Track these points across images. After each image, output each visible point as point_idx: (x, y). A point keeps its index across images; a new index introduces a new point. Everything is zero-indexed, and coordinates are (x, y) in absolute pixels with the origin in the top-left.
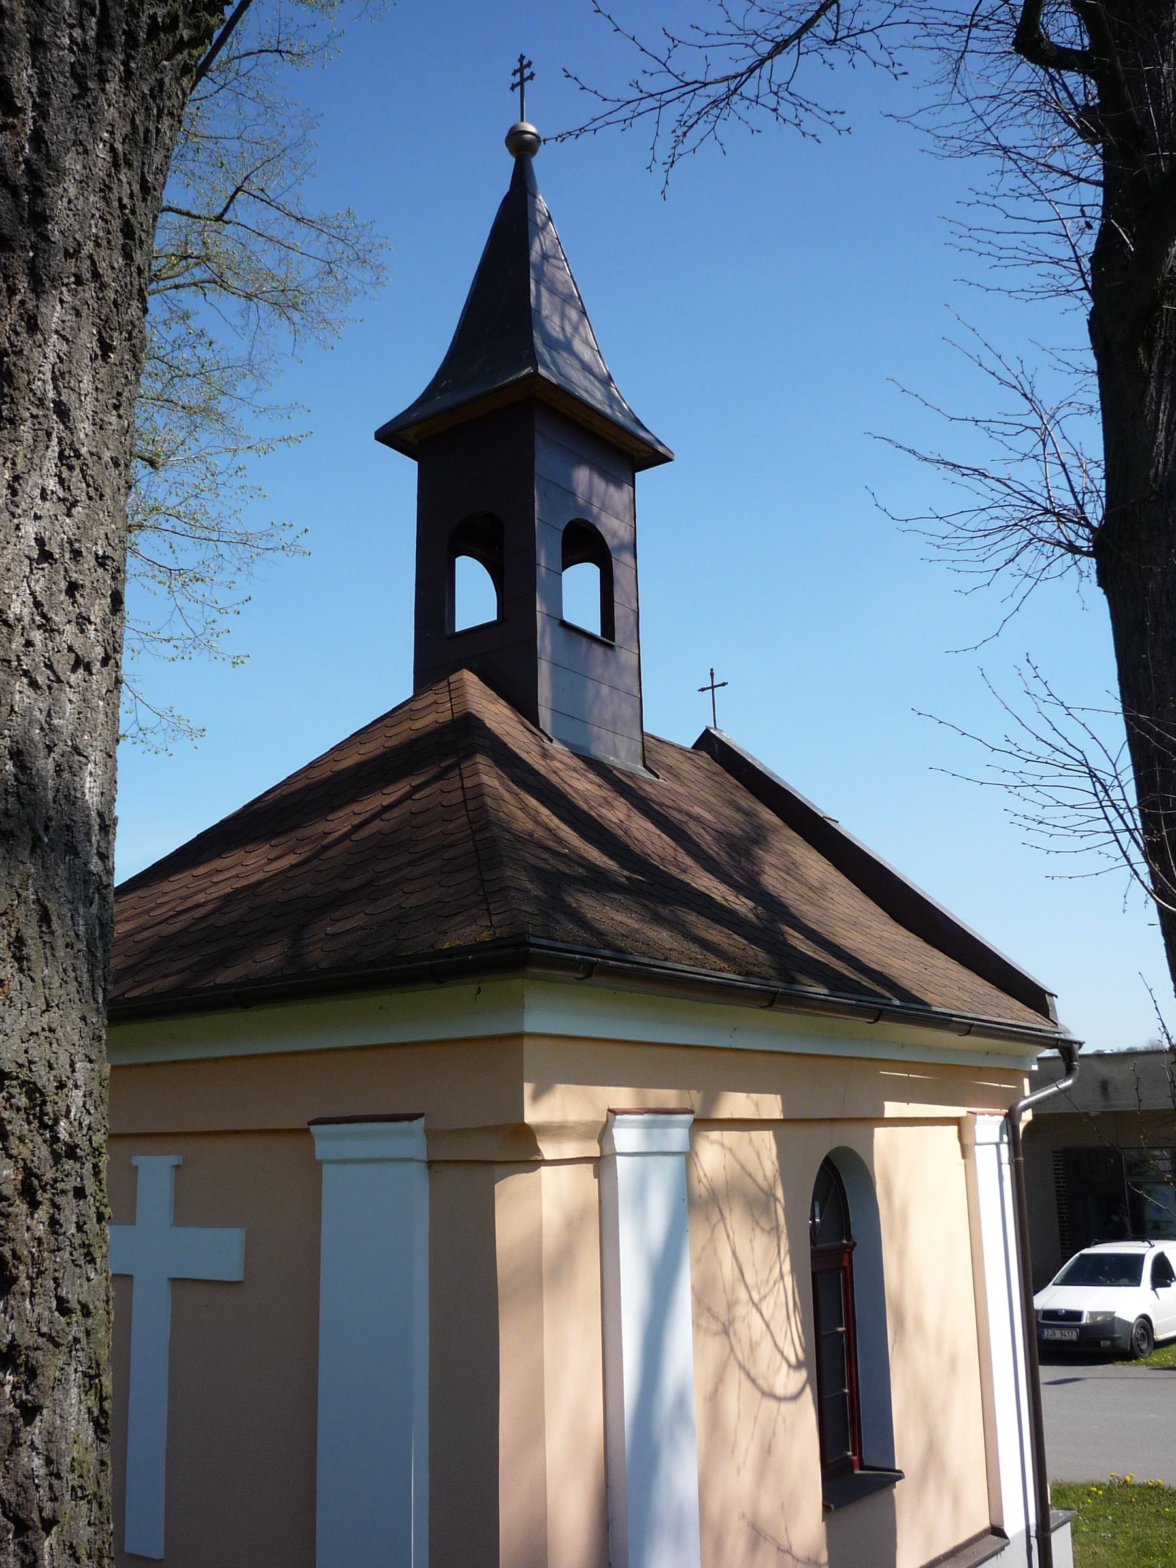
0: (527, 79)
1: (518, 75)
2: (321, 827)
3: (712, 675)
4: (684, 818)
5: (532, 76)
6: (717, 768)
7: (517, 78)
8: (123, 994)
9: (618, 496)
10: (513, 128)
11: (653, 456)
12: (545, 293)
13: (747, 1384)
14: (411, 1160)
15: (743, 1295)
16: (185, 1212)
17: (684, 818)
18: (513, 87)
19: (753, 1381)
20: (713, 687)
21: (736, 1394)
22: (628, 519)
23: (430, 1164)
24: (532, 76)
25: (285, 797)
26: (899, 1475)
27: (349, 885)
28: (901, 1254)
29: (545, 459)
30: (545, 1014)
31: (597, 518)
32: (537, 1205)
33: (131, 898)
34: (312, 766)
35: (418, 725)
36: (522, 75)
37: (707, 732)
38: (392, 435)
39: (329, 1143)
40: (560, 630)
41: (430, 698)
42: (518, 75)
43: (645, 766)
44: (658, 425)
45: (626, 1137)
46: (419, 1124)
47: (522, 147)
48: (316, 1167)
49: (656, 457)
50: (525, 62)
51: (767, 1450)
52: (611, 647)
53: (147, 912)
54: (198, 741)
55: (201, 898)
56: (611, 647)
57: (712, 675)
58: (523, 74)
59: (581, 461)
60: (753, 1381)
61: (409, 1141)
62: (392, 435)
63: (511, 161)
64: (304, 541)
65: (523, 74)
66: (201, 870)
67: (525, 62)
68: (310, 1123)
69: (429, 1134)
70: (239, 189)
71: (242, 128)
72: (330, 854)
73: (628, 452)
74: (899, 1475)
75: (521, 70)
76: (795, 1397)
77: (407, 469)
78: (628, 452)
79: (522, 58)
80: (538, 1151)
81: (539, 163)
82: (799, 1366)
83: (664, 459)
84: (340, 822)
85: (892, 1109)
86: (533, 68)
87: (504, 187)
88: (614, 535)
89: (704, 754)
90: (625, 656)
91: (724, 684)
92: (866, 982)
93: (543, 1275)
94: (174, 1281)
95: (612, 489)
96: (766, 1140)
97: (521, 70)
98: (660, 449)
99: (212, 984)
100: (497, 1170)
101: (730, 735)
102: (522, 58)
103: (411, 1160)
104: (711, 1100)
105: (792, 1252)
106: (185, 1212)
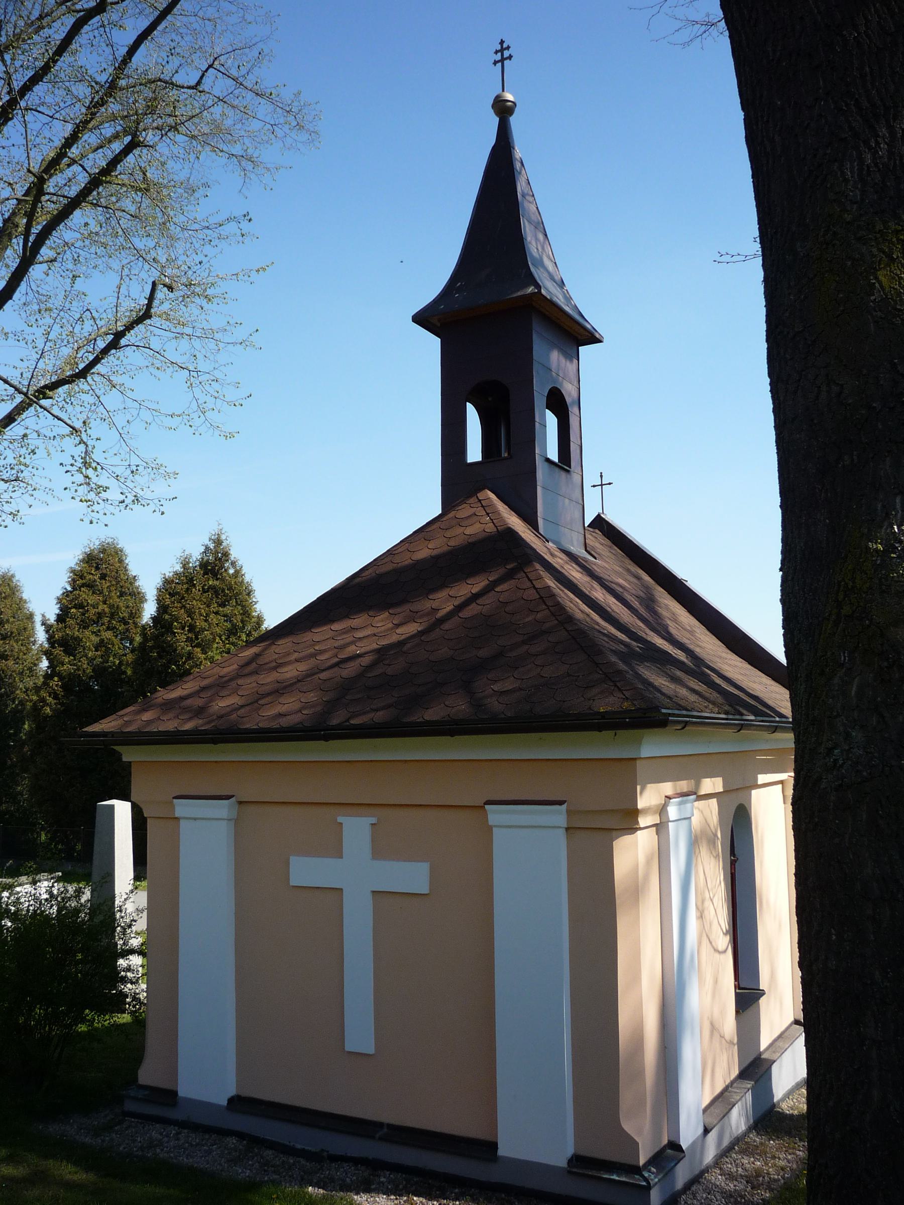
0: (506, 59)
1: (499, 54)
2: (426, 605)
3: (601, 476)
4: (621, 590)
5: (510, 57)
6: (608, 542)
7: (498, 57)
8: (348, 720)
9: (571, 367)
10: (498, 97)
11: (592, 338)
12: (527, 223)
13: (709, 944)
14: (560, 827)
15: (707, 896)
16: (379, 851)
17: (621, 590)
18: (495, 63)
19: (711, 943)
20: (602, 485)
21: (706, 948)
22: (576, 383)
23: (567, 829)
24: (510, 57)
25: (381, 576)
26: (762, 993)
27: (484, 653)
28: (761, 863)
29: (538, 347)
30: (653, 746)
31: (561, 384)
32: (632, 852)
33: (284, 644)
34: (390, 553)
35: (469, 531)
36: (502, 55)
37: (599, 516)
38: (422, 319)
39: (496, 815)
40: (546, 464)
41: (464, 511)
42: (499, 54)
43: (586, 550)
44: (595, 319)
45: (673, 811)
46: (564, 807)
47: (503, 110)
48: (489, 830)
49: (592, 338)
50: (505, 45)
51: (716, 981)
52: (568, 471)
53: (313, 655)
54: (171, 481)
55: (352, 650)
56: (568, 471)
57: (601, 476)
58: (503, 55)
59: (554, 346)
60: (711, 943)
61: (557, 816)
62: (422, 319)
63: (496, 120)
64: (255, 338)
65: (503, 55)
66: (336, 626)
67: (505, 45)
68: (486, 803)
69: (569, 812)
70: (210, 66)
71: (199, 7)
72: (447, 626)
73: (576, 334)
74: (762, 993)
75: (502, 50)
76: (725, 951)
77: (431, 345)
78: (576, 334)
79: (502, 42)
80: (638, 823)
81: (514, 121)
82: (725, 934)
83: (599, 341)
84: (443, 601)
85: (762, 779)
86: (511, 51)
87: (492, 141)
88: (570, 395)
89: (597, 531)
90: (576, 478)
91: (610, 484)
92: (760, 707)
93: (637, 892)
94: (373, 892)
95: (568, 363)
96: (714, 802)
97: (502, 50)
98: (597, 336)
99: (421, 720)
100: (614, 833)
101: (611, 517)
102: (502, 42)
103: (560, 827)
104: (698, 785)
105: (724, 868)
106: (379, 851)
